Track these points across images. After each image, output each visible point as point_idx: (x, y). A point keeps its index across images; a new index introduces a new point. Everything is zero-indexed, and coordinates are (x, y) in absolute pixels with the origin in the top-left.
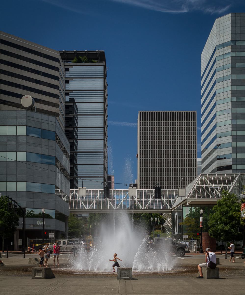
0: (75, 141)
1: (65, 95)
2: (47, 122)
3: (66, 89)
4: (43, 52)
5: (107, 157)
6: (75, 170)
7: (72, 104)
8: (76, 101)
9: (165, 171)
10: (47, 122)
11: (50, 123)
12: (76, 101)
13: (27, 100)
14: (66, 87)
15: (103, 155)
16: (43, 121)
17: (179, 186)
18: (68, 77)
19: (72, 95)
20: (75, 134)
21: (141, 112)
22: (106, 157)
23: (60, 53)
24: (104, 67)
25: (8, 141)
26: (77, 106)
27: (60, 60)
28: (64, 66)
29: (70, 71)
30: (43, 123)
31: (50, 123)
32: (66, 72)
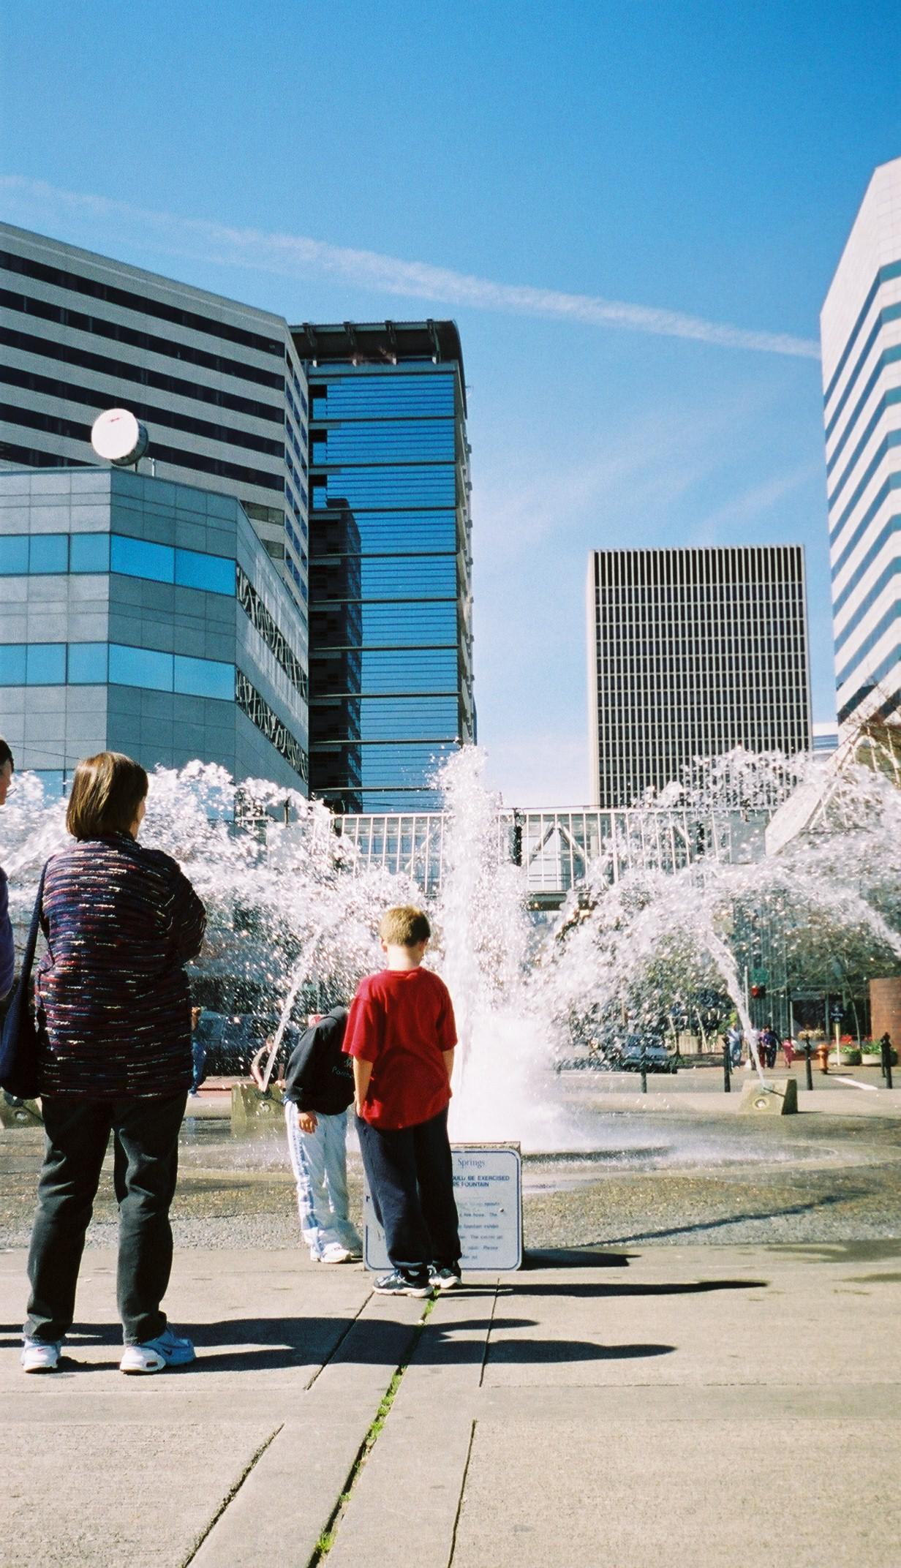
0: (350, 655)
1: (311, 486)
2: (198, 518)
3: (316, 461)
4: (227, 321)
5: (474, 716)
6: (351, 762)
7: (337, 517)
8: (352, 506)
9: (676, 600)
10: (198, 518)
11: (211, 522)
12: (352, 506)
13: (115, 434)
14: (315, 454)
15: (456, 707)
16: (181, 515)
17: (736, 739)
18: (324, 417)
19: (335, 487)
20: (349, 630)
21: (596, 555)
22: (469, 716)
23: (293, 335)
24: (455, 381)
25: (34, 598)
26: (360, 530)
27: (290, 347)
28: (309, 377)
29: (329, 395)
30: (183, 524)
31: (211, 522)
32: (315, 401)
